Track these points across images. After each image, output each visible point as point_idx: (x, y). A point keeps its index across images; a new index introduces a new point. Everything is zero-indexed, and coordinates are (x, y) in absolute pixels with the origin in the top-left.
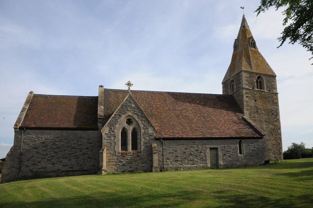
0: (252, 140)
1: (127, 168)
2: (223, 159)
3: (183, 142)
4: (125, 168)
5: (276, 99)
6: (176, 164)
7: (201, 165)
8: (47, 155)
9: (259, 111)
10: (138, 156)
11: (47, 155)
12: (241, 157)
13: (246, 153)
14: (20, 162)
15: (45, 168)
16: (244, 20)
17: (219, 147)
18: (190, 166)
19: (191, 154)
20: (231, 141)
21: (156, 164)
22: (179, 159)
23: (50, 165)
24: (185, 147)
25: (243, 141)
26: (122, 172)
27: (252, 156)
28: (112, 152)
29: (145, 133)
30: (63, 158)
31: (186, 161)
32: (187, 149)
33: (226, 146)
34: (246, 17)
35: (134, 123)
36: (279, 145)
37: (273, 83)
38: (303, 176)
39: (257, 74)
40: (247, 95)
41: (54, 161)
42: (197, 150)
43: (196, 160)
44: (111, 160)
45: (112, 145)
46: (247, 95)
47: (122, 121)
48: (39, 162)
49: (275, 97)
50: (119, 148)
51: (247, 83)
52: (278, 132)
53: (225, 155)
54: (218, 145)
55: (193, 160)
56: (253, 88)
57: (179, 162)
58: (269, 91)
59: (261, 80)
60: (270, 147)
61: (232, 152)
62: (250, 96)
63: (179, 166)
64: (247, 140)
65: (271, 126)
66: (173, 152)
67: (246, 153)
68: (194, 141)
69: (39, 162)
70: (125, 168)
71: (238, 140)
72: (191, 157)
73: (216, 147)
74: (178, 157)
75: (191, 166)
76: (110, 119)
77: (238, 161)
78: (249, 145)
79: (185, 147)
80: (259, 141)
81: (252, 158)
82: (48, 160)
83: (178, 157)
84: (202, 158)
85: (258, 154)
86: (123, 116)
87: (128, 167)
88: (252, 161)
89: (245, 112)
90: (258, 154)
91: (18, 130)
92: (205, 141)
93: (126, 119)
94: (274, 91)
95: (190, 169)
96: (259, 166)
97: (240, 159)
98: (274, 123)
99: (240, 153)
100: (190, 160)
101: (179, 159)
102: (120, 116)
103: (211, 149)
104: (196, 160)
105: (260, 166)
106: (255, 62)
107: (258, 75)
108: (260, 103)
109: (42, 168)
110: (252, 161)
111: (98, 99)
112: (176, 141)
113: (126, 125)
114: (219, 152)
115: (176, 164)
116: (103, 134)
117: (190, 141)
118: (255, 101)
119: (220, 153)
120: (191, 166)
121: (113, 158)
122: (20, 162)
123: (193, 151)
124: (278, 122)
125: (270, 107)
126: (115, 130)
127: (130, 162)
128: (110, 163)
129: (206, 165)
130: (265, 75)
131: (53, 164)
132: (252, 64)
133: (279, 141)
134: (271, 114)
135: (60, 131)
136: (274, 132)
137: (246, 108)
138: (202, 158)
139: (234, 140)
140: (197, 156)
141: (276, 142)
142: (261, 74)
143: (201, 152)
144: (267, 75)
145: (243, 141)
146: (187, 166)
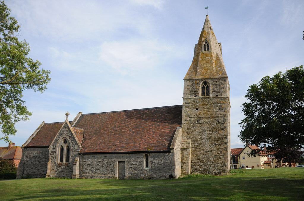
0: (158, 154)
1: (61, 174)
2: (129, 171)
3: (97, 156)
4: (60, 174)
5: (225, 104)
6: (92, 174)
7: (110, 175)
8: (35, 164)
9: (200, 121)
10: (68, 166)
11: (35, 164)
12: (146, 170)
13: (151, 166)
14: (24, 168)
15: (34, 172)
16: (206, 21)
17: (126, 160)
18: (101, 175)
19: (103, 166)
20: (138, 155)
21: (77, 171)
22: (94, 169)
23: (37, 171)
24: (99, 160)
25: (149, 155)
26: (58, 177)
27: (158, 169)
28: (54, 163)
29: (73, 150)
30: (43, 166)
31: (99, 171)
32: (100, 161)
33: (132, 159)
34: (209, 18)
35: (68, 142)
36: (224, 156)
37: (222, 86)
38: (217, 197)
39: (202, 80)
40: (187, 105)
41: (39, 168)
42: (107, 163)
43: (106, 171)
44: (53, 169)
45: (54, 158)
46: (187, 105)
47: (61, 141)
48: (32, 169)
49: (223, 101)
50: (58, 161)
51: (189, 91)
52: (223, 141)
53: (131, 167)
54: (126, 159)
55: (104, 171)
56: (195, 96)
57: (94, 172)
58: (217, 96)
59: (209, 86)
60: (211, 158)
61: (138, 166)
62: (191, 105)
63: (94, 175)
64: (153, 154)
65: (214, 135)
66: (90, 164)
67: (151, 166)
68: (105, 155)
69: (32, 169)
70: (60, 174)
71: (144, 154)
72: (103, 168)
73: (123, 160)
74: (93, 168)
75: (102, 175)
76: (54, 140)
77: (143, 173)
78: (155, 159)
79: (99, 160)
80: (167, 154)
81: (157, 172)
82: (36, 167)
83: (93, 168)
84: (111, 170)
85: (165, 168)
86: (61, 138)
87: (62, 174)
88: (157, 174)
89: (182, 123)
90: (165, 168)
91: (23, 149)
92: (114, 155)
93: (63, 140)
94: (224, 95)
95: (101, 178)
96: (164, 179)
97: (145, 172)
98: (219, 132)
99: (147, 166)
100: (102, 171)
101: (94, 169)
102: (59, 138)
103: (119, 162)
104: (106, 171)
105: (165, 179)
106: (202, 66)
107: (203, 81)
108: (202, 112)
109: (33, 172)
110: (157, 174)
111: (182, 107)
112: (93, 155)
113: (63, 143)
114: (126, 165)
115: (92, 174)
116: (50, 151)
117: (102, 155)
118: (197, 109)
119: (127, 166)
120: (102, 175)
121: (54, 167)
122: (24, 168)
123: (104, 164)
124: (225, 129)
125: (216, 113)
126: (56, 148)
127: (63, 171)
128: (52, 171)
129: (114, 175)
130: (212, 79)
131: (38, 170)
132: (199, 70)
133: (224, 152)
134: (216, 121)
135: (42, 148)
136: (217, 142)
137: (184, 118)
138: (111, 170)
139: (140, 154)
140: (107, 168)
141: (220, 153)
142: (207, 79)
143: (110, 165)
144: (214, 78)
145: (149, 155)
146: (99, 175)
